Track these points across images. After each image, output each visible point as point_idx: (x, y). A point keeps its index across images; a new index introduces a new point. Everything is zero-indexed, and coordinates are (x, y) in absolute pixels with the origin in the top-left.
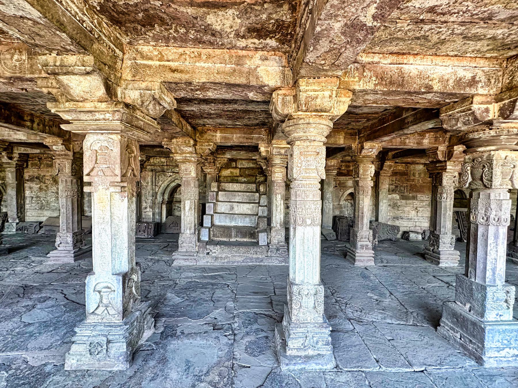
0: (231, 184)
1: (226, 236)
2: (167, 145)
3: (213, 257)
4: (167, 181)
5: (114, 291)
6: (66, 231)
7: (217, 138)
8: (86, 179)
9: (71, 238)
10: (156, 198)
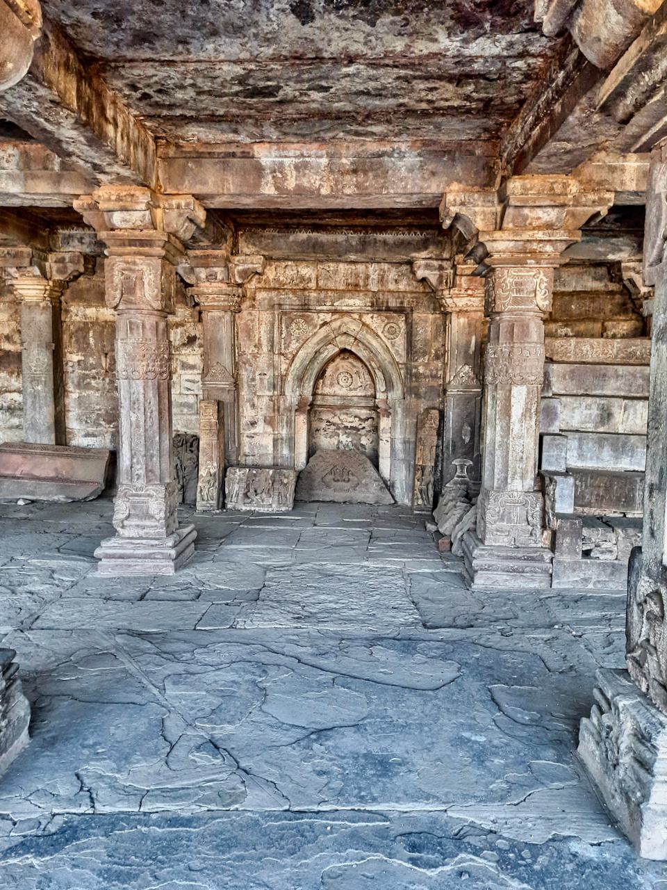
0: (573, 341)
1: (616, 502)
2: (463, 204)
3: (604, 565)
4: (315, 340)
10: (282, 394)
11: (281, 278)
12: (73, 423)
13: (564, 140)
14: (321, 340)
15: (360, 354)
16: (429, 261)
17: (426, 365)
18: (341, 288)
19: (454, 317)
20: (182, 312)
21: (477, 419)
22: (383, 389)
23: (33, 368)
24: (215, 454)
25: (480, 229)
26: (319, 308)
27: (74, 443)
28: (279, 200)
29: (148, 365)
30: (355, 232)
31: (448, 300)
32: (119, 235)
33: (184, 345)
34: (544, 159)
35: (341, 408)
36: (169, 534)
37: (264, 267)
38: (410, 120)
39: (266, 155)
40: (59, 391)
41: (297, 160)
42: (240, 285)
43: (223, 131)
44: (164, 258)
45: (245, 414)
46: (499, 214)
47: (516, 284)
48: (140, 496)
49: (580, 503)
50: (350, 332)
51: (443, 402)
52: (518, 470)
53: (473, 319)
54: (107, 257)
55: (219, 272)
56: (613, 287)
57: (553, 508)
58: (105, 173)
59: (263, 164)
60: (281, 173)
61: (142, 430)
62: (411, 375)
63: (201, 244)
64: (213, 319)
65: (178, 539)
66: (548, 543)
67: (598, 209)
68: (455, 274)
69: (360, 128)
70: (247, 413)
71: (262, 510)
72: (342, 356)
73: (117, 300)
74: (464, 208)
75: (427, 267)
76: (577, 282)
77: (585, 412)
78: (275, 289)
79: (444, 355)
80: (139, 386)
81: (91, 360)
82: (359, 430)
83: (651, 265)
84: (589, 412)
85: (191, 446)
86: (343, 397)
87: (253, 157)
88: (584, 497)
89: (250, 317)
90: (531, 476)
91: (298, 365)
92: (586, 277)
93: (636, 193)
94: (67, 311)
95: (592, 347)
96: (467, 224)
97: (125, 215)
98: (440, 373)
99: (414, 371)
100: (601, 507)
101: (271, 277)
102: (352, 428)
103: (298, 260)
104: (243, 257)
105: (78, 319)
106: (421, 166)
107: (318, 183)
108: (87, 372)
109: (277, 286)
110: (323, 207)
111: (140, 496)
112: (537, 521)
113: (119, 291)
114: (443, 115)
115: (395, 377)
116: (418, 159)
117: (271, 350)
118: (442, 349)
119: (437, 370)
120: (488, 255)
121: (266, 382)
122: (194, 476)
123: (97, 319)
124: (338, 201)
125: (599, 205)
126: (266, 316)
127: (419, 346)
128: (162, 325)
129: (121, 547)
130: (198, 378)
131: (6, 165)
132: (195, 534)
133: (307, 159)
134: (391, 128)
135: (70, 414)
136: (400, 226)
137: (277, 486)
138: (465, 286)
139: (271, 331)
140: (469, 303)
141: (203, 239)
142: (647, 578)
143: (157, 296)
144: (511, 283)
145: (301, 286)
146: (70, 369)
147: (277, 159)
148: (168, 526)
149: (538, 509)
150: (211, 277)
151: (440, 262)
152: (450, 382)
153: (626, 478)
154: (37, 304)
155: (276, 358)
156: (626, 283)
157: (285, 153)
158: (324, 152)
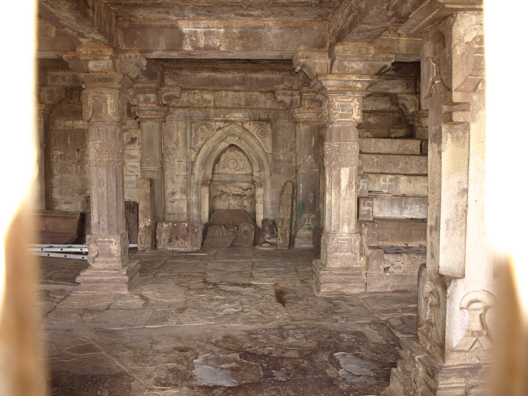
0: (373, 140)
2: (307, 58)
3: (396, 276)
5: (462, 308)
6: (107, 232)
7: (401, 46)
8: (457, 97)
10: (192, 173)
11: (192, 101)
13: (367, 24)
15: (242, 148)
16: (284, 91)
17: (285, 155)
18: (230, 106)
20: (130, 122)
24: (149, 214)
25: (318, 72)
26: (216, 119)
28: (194, 53)
30: (238, 73)
31: (297, 115)
33: (129, 143)
34: (355, 34)
36: (124, 266)
37: (181, 93)
38: (275, 8)
39: (186, 28)
41: (205, 30)
42: (165, 105)
43: (159, 13)
44: (120, 90)
45: (169, 187)
46: (329, 64)
47: (341, 106)
48: (105, 242)
50: (235, 134)
51: (296, 178)
54: (84, 89)
55: (152, 97)
56: (394, 108)
59: (184, 32)
60: (195, 37)
61: (105, 199)
62: (276, 161)
66: (364, 263)
67: (386, 63)
68: (301, 99)
69: (245, 12)
70: (170, 187)
71: (181, 250)
72: (230, 149)
74: (308, 60)
75: (284, 94)
76: (372, 105)
80: (103, 172)
83: (426, 98)
84: (385, 183)
86: (232, 175)
87: (178, 28)
89: (171, 125)
93: (407, 55)
94: (53, 123)
95: (384, 144)
96: (309, 70)
97: (97, 63)
98: (294, 159)
99: (277, 158)
100: (393, 241)
101: (185, 100)
102: (238, 195)
103: (201, 90)
104: (168, 88)
105: (60, 128)
106: (281, 35)
107: (218, 44)
109: (189, 105)
114: (295, 6)
115: (265, 163)
116: (280, 31)
120: (323, 88)
123: (73, 128)
124: (231, 54)
125: (387, 61)
126: (181, 124)
128: (118, 131)
129: (93, 275)
130: (138, 164)
133: (212, 30)
134: (263, 12)
135: (55, 189)
136: (266, 70)
137: (190, 233)
138: (307, 106)
139: (185, 134)
141: (143, 77)
142: (429, 283)
143: (116, 113)
145: (204, 105)
146: (55, 160)
149: (357, 244)
150: (147, 100)
151: (291, 92)
152: (299, 166)
155: (188, 150)
156: (401, 106)
158: (222, 25)
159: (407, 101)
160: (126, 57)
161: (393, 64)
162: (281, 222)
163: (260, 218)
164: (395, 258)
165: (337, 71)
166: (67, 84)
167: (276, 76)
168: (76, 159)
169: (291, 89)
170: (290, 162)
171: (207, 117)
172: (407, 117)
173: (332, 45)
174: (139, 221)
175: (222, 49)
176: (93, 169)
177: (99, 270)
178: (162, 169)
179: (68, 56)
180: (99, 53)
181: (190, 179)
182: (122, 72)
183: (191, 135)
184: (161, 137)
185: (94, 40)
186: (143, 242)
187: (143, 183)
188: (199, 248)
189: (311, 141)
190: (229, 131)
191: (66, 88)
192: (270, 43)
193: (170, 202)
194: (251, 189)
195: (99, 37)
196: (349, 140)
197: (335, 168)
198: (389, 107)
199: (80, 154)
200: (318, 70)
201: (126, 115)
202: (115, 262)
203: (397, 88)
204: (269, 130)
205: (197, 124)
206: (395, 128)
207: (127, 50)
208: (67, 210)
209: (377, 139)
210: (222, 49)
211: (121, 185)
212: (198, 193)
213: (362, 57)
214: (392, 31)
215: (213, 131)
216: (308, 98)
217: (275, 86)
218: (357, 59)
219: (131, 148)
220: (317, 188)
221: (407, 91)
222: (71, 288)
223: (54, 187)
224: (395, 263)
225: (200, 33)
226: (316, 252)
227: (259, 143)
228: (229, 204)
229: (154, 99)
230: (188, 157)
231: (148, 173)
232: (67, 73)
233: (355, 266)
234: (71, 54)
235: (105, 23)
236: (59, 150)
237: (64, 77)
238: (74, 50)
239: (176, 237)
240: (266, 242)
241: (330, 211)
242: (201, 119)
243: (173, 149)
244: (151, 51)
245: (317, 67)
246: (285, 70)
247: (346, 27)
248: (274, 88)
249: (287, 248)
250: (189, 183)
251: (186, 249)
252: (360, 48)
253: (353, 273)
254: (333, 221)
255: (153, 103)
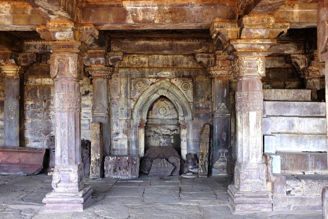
0: (273, 90)
1: (299, 168)
2: (221, 27)
3: (297, 198)
4: (148, 91)
6: (67, 163)
7: (294, 16)
9: (76, 173)
10: (132, 118)
11: (131, 62)
12: (28, 136)
14: (151, 92)
15: (170, 98)
17: (203, 103)
19: (216, 80)
21: (229, 129)
22: (182, 115)
23: (10, 109)
25: (230, 38)
26: (150, 76)
27: (28, 145)
28: (134, 26)
29: (70, 105)
31: (212, 72)
32: (57, 43)
35: (161, 125)
36: (80, 190)
37: (123, 56)
40: (22, 119)
41: (143, 8)
42: (111, 66)
44: (78, 54)
45: (114, 129)
46: (239, 32)
47: (248, 63)
48: (66, 171)
49: (283, 168)
52: (255, 153)
53: (224, 80)
54: (52, 53)
55: (102, 59)
56: (288, 65)
57: (272, 171)
58: (53, 14)
60: (136, 13)
61: (66, 137)
62: (197, 108)
63: (94, 47)
64: (98, 82)
65: (84, 193)
67: (283, 30)
68: (216, 60)
70: (115, 129)
71: (123, 178)
73: (56, 74)
74: (222, 29)
75: (202, 56)
77: (282, 124)
78: (128, 67)
79: (211, 98)
80: (65, 116)
81: (38, 104)
82: (170, 136)
83: (322, 53)
84: (284, 124)
85: (86, 146)
86: (162, 120)
87: (123, 6)
88: (285, 165)
89: (116, 81)
90: (260, 155)
91: (139, 104)
92: (275, 62)
93: (299, 23)
94: (27, 81)
95: (282, 93)
96: (223, 37)
98: (210, 106)
101: (126, 62)
102: (166, 135)
103: (139, 54)
105: (32, 84)
107: (153, 18)
108: (35, 110)
109: (129, 66)
110: (155, 29)
111: (66, 171)
112: (264, 178)
113: (57, 70)
115: (188, 109)
117: (126, 97)
118: (211, 95)
119: (208, 105)
120: (234, 50)
121: (124, 113)
122: (88, 160)
123: (41, 84)
124: (163, 26)
126: (124, 81)
127: (199, 94)
128: (77, 85)
129: (56, 197)
130: (90, 111)
131: (4, 12)
132: (92, 190)
133: (148, 7)
135: (27, 131)
136: (189, 38)
137: (130, 165)
138: (220, 65)
139: (126, 88)
140: (223, 73)
141: (95, 45)
143: (75, 71)
144: (246, 63)
145: (141, 66)
146: (27, 109)
147: (134, 7)
148: (79, 187)
149: (264, 172)
150: (98, 62)
151: (208, 54)
152: (215, 111)
153: (304, 155)
154: (13, 77)
155: (129, 100)
157: (138, 5)
158: (156, 4)
159: (299, 59)
160: (83, 29)
161: (288, 30)
162: (201, 156)
163: (184, 153)
164: (295, 183)
165: (244, 37)
166: (38, 51)
167: (196, 43)
168: (43, 108)
169: (207, 52)
170: (207, 109)
171: (143, 74)
172: (299, 72)
173: (240, 17)
174: (91, 155)
175: (156, 22)
176: (58, 114)
177: (61, 193)
178: (109, 115)
179: (40, 28)
180: (64, 27)
181: (130, 123)
182: (81, 40)
183: (131, 89)
184: (108, 91)
185: (60, 16)
186: (94, 170)
187: (94, 126)
188: (137, 177)
189: (223, 92)
190: (160, 85)
191: (37, 54)
192: (193, 16)
193: (115, 140)
194: (177, 130)
195: (64, 14)
196: (255, 89)
197: (245, 112)
198: (284, 65)
199: (46, 104)
200: (230, 36)
201: (82, 73)
202: (73, 186)
203: (290, 50)
204: (191, 84)
205: (135, 80)
206: (289, 81)
207: (84, 24)
208: (36, 147)
209: (276, 90)
210: (156, 22)
211: (78, 127)
212: (136, 133)
213: (264, 25)
214: (287, 5)
215: (148, 85)
216: (221, 59)
217: (195, 51)
218: (261, 27)
219: (85, 99)
220: (229, 129)
221: (298, 52)
222: (38, 207)
223: (26, 129)
224: (295, 187)
225: (140, 10)
226: (230, 178)
227: (182, 93)
228: (160, 142)
229: (103, 61)
230: (128, 105)
231: (98, 118)
232: (38, 42)
233: (263, 190)
234: (42, 28)
235: (68, 3)
236: (31, 101)
237: (36, 46)
238: (45, 25)
239: (120, 168)
240: (189, 172)
241: (242, 146)
242: (138, 76)
243: (118, 100)
244: (102, 25)
245: (229, 34)
246: (203, 38)
247: (252, 2)
248: (194, 52)
249: (207, 177)
250: (129, 125)
251: (127, 177)
252: (263, 18)
253: (261, 196)
254: (244, 154)
255: (102, 64)
